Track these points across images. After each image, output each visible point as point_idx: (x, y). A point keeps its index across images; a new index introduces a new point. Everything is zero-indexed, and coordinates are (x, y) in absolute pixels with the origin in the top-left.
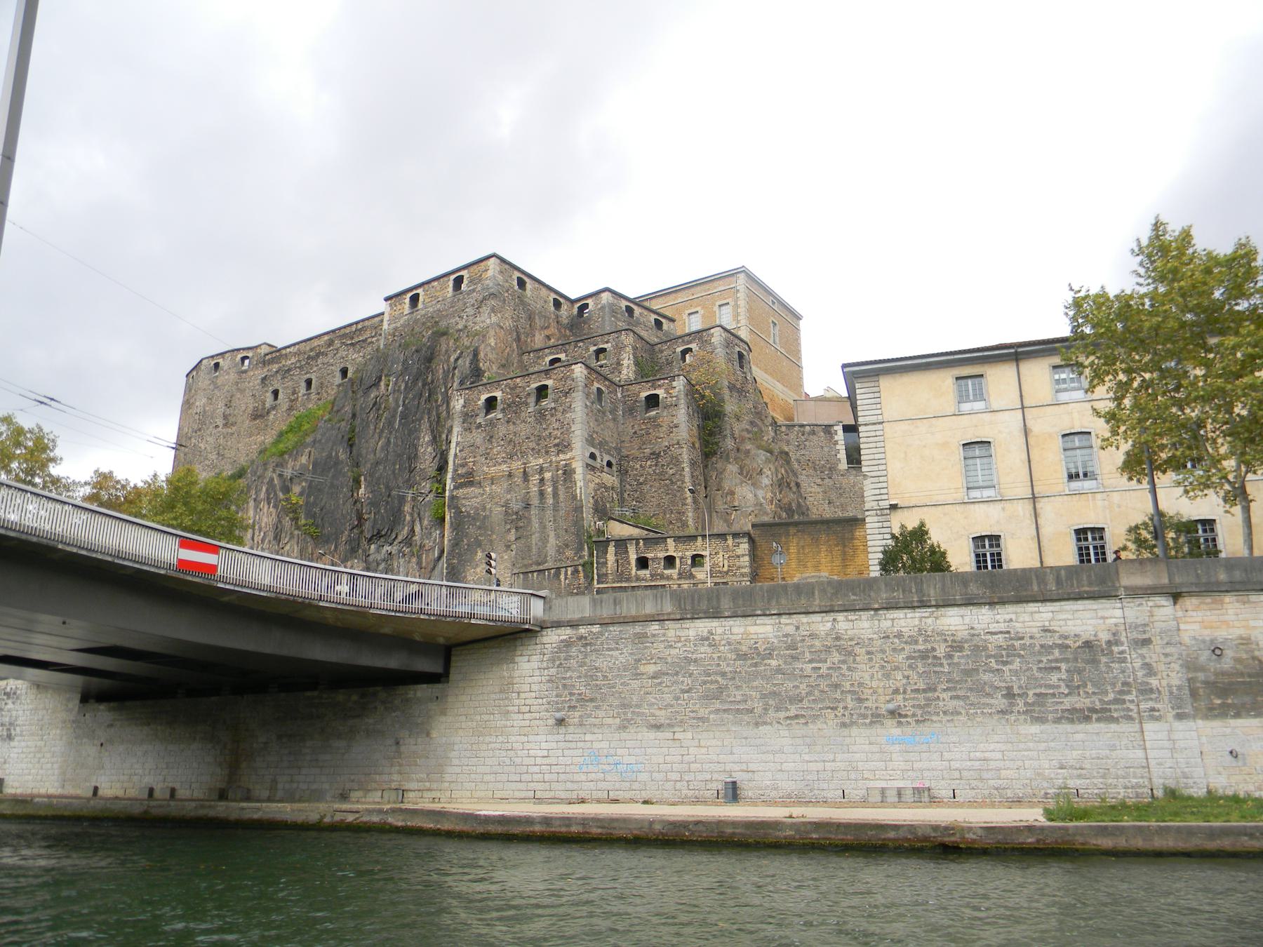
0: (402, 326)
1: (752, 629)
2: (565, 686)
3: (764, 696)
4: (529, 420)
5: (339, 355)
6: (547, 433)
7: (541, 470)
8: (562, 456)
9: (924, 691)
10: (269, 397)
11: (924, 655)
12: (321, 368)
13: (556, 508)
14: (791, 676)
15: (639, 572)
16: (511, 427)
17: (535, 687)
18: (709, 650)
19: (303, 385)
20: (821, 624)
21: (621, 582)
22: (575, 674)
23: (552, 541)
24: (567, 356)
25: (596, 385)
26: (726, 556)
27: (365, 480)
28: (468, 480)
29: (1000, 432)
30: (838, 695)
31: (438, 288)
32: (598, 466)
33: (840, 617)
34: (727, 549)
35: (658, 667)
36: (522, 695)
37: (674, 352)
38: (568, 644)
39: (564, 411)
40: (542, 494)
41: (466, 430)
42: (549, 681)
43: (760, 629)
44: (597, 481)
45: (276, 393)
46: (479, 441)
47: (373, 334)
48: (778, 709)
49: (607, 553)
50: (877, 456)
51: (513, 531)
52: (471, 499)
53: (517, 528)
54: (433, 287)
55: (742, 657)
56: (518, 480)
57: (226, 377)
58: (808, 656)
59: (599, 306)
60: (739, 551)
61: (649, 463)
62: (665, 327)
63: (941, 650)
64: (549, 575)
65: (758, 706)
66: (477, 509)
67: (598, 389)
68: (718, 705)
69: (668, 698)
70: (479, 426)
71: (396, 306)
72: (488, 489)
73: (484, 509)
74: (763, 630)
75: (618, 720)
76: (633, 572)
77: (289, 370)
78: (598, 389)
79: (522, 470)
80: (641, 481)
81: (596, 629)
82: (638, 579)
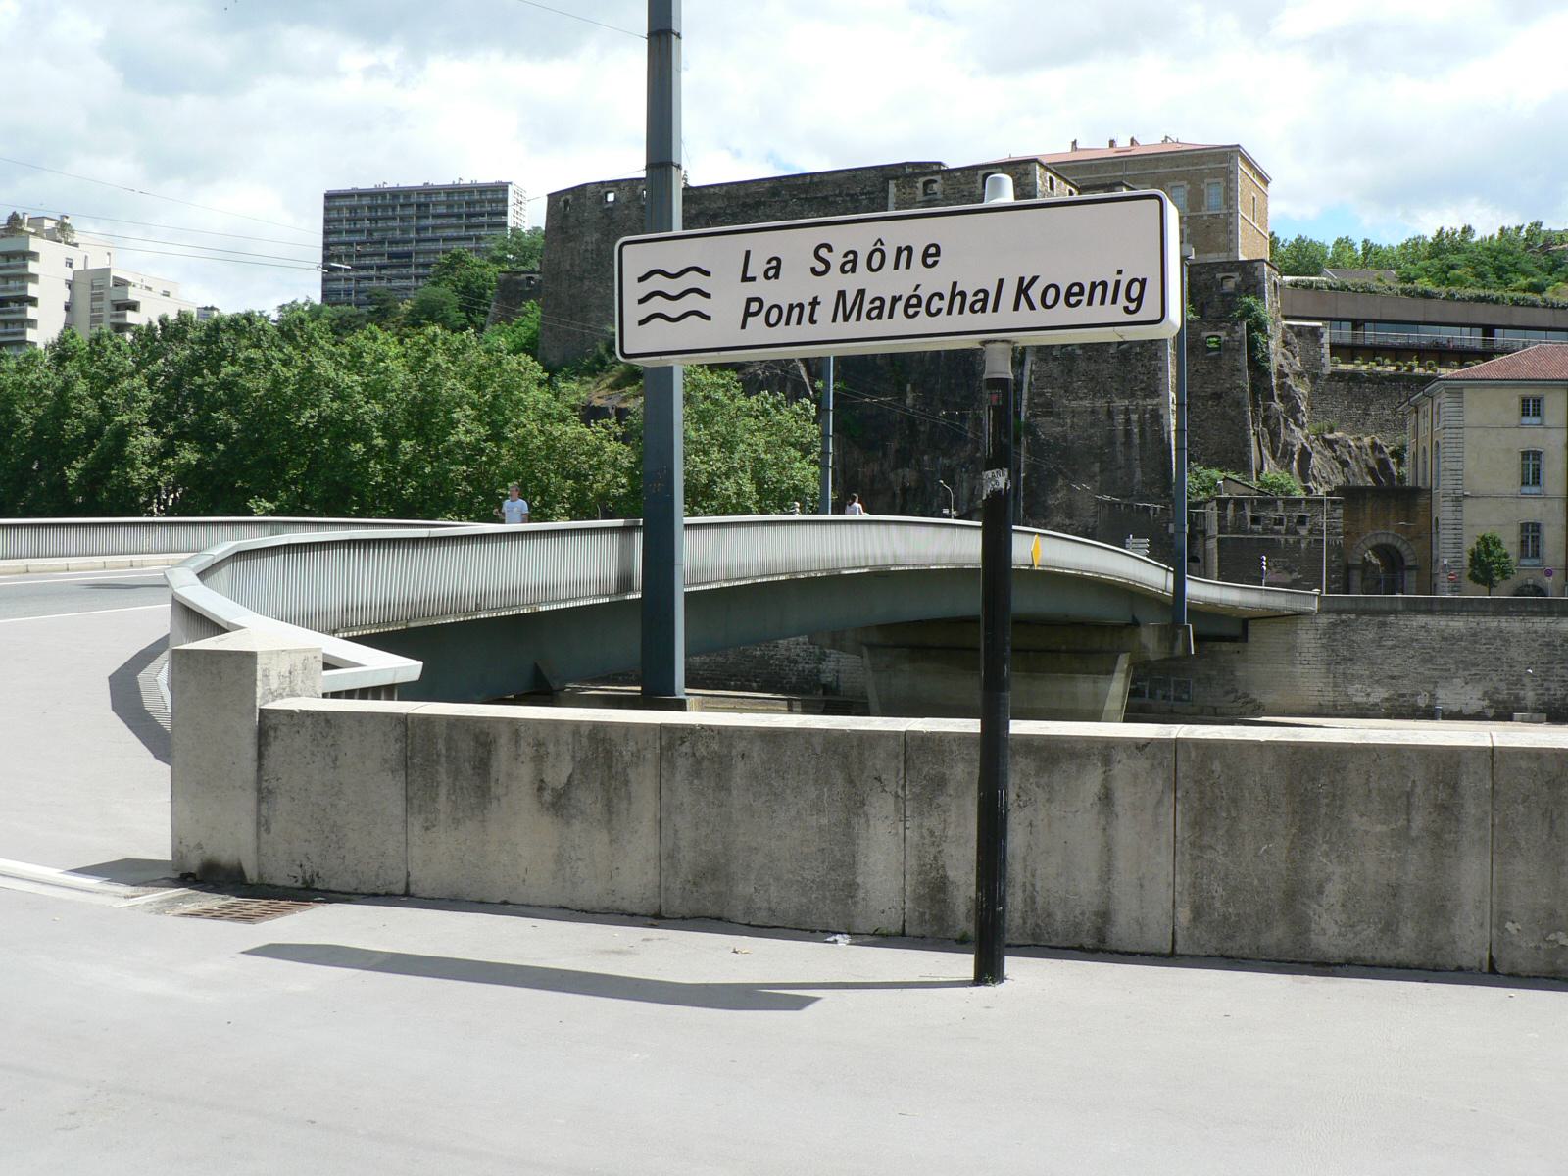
1: (1451, 624)
2: (1333, 650)
3: (1457, 662)
4: (1112, 360)
7: (1127, 411)
8: (1148, 401)
9: (1548, 664)
11: (1548, 644)
13: (1143, 444)
14: (1474, 652)
15: (1254, 527)
16: (1093, 366)
18: (1425, 634)
20: (1492, 623)
22: (1340, 643)
23: (1138, 475)
28: (1048, 409)
29: (1550, 445)
30: (1499, 663)
33: (1503, 619)
36: (1304, 654)
37: (1215, 277)
38: (1334, 625)
39: (1150, 358)
40: (1128, 433)
41: (1041, 359)
42: (1323, 647)
43: (1457, 624)
46: (1056, 372)
47: (837, 192)
48: (1464, 670)
50: (1457, 454)
51: (1097, 464)
53: (1101, 462)
54: (955, 178)
55: (1444, 639)
57: (626, 212)
58: (1483, 641)
60: (1335, 515)
61: (1210, 402)
63: (1558, 642)
66: (1057, 439)
71: (903, 187)
72: (1069, 421)
75: (1367, 673)
79: (1106, 408)
80: (1203, 418)
81: (1353, 617)
82: (1252, 532)
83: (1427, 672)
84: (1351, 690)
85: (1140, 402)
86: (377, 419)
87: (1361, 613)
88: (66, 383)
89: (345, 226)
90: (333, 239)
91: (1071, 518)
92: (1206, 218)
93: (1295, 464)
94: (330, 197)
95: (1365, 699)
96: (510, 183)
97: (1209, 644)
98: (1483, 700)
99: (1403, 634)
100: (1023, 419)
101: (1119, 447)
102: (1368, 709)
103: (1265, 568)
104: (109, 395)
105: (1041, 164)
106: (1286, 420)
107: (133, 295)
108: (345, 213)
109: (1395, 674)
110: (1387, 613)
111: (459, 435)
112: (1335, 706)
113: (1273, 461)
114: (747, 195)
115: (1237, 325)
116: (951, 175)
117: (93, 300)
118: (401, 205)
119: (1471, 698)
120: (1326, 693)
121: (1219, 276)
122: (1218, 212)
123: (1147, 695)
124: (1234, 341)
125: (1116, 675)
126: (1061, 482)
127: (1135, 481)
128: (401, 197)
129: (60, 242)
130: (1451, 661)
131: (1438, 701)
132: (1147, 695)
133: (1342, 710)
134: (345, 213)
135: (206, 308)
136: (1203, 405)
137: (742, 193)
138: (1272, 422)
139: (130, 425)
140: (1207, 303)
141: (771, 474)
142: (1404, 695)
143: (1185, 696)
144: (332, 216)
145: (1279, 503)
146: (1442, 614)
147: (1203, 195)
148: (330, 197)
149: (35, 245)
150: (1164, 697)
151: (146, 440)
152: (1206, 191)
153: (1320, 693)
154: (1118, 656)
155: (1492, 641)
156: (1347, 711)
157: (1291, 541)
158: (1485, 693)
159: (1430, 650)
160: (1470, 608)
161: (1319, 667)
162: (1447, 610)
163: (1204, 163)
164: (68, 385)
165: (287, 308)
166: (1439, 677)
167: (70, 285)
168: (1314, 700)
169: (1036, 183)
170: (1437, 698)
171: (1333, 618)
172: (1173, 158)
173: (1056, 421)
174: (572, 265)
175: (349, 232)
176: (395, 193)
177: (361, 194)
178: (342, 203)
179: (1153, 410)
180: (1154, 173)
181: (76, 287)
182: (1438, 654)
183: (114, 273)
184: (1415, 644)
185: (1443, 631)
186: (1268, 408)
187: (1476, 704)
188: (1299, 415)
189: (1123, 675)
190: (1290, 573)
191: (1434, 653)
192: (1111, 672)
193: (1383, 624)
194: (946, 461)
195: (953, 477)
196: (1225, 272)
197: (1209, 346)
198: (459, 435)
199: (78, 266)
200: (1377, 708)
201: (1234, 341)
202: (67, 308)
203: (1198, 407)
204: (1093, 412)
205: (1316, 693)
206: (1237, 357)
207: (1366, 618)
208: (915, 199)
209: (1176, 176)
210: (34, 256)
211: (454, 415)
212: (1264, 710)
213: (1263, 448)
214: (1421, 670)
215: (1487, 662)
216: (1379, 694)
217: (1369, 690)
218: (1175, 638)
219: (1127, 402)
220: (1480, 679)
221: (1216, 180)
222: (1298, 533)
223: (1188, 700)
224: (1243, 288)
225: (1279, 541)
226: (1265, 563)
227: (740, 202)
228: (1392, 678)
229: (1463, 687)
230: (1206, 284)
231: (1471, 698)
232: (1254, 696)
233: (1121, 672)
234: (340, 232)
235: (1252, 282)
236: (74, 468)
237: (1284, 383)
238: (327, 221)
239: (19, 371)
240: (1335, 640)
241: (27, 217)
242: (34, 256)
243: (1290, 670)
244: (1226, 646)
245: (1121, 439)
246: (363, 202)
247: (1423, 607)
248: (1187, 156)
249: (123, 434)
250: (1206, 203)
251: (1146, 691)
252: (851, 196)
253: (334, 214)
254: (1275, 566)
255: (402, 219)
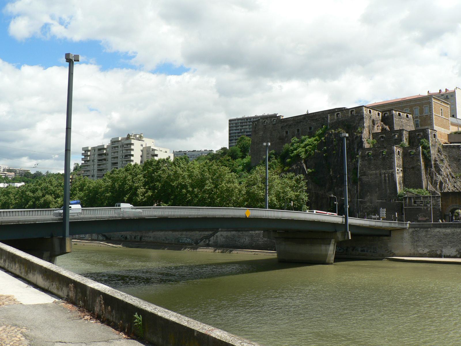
0: (334, 122)
1: (446, 230)
2: (413, 238)
5: (308, 123)
6: (386, 163)
7: (385, 174)
8: (390, 170)
10: (285, 133)
12: (302, 126)
14: (453, 239)
17: (408, 238)
18: (439, 234)
19: (296, 131)
21: (410, 207)
23: (388, 191)
24: (385, 136)
25: (398, 150)
26: (435, 201)
27: (332, 170)
28: (364, 174)
31: (346, 113)
32: (399, 172)
34: (435, 200)
35: (430, 236)
37: (416, 134)
38: (413, 231)
39: (390, 159)
40: (385, 180)
43: (448, 231)
44: (399, 176)
45: (287, 132)
47: (319, 117)
48: (451, 244)
49: (406, 200)
51: (378, 189)
52: (365, 179)
54: (344, 112)
55: (444, 235)
56: (378, 175)
57: (269, 126)
58: (456, 235)
59: (391, 114)
61: (411, 170)
62: (409, 117)
64: (388, 200)
65: (447, 243)
67: (398, 151)
68: (440, 242)
69: (432, 241)
70: (366, 160)
71: (332, 116)
72: (370, 177)
73: (369, 182)
74: (448, 231)
76: (413, 204)
77: (291, 125)
78: (398, 151)
81: (419, 229)
82: (414, 206)
83: (440, 244)
84: (419, 249)
85: (388, 171)
86: (189, 184)
87: (421, 228)
88: (126, 177)
89: (234, 128)
90: (232, 132)
91: (371, 204)
92: (424, 116)
93: (438, 186)
94: (230, 121)
95: (422, 252)
96: (277, 114)
97: (381, 237)
98: (456, 252)
99: (433, 234)
100: (358, 177)
101: (383, 184)
102: (423, 255)
103: (397, 216)
104: (135, 179)
105: (365, 107)
106: (435, 173)
107: (156, 153)
108: (234, 125)
109: (431, 245)
110: (428, 228)
111: (207, 187)
112: (414, 254)
113: (431, 186)
114: (298, 120)
115: (418, 148)
116: (343, 111)
117: (147, 154)
118: (249, 122)
119: (453, 252)
120: (411, 250)
121: (417, 134)
122: (427, 114)
123: (366, 251)
124: (417, 152)
125: (331, 245)
126: (368, 194)
127: (388, 193)
128: (249, 119)
129: (140, 140)
130: (446, 241)
131: (443, 252)
132: (366, 251)
133: (416, 255)
134: (234, 125)
135: (210, 151)
136: (409, 170)
137: (296, 119)
138: (431, 175)
139: (138, 186)
140: (414, 142)
141: (282, 195)
142: (433, 251)
143: (375, 252)
144: (231, 126)
145: (421, 197)
146: (444, 228)
147: (423, 110)
148: (230, 121)
149: (133, 141)
150: (370, 252)
151: (142, 190)
152: (414, 110)
153: (410, 250)
154: (331, 240)
155: (459, 235)
156: (418, 256)
157: (425, 208)
158: (457, 250)
159: (440, 238)
160: (452, 226)
161: (410, 243)
162: (445, 227)
163: (423, 101)
164: (126, 177)
165: (218, 151)
166: (443, 246)
167: (142, 151)
168: (408, 252)
169: (363, 113)
170: (443, 252)
171: (413, 229)
172: (414, 100)
173: (367, 177)
174: (257, 141)
175: (235, 130)
176: (247, 119)
177: (238, 119)
178: (233, 122)
179: (391, 173)
180: (399, 107)
181: (144, 151)
182: (442, 239)
183: (152, 147)
184: (436, 236)
185: (444, 232)
186: (430, 170)
187: (454, 253)
188: (440, 172)
189: (333, 245)
190: (425, 217)
191: (441, 239)
192: (329, 244)
193: (427, 231)
194: (340, 189)
195: (342, 193)
196: (418, 133)
197: (411, 154)
198: (207, 187)
199: (144, 146)
200: (426, 254)
201: (417, 152)
202: (141, 156)
203: (408, 171)
204: (376, 174)
205: (409, 250)
206: (418, 157)
207: (422, 229)
208: (334, 118)
209: (405, 107)
210: (133, 144)
211: (206, 182)
212: (395, 255)
213: (428, 182)
214: (438, 244)
215: (457, 242)
216: (426, 251)
217: (423, 249)
218: (345, 235)
219: (384, 171)
220: (455, 246)
221: (427, 105)
222: (427, 206)
223: (376, 253)
224: (423, 137)
225: (422, 208)
226: (397, 215)
227: (296, 122)
228: (430, 246)
229: (450, 248)
230: (414, 136)
231: (453, 252)
232: (393, 251)
233: (333, 244)
234: (233, 130)
235: (426, 135)
236: (126, 197)
237: (436, 163)
238: (230, 127)
239: (117, 174)
240: (414, 236)
241: (133, 134)
242: (133, 144)
243: (402, 244)
244: (386, 238)
245: (383, 181)
246: (239, 122)
247: (438, 226)
248: (418, 99)
249: (136, 188)
250: (424, 112)
251: (366, 250)
252: (323, 118)
253: (232, 125)
254: (421, 216)
255: (249, 125)
